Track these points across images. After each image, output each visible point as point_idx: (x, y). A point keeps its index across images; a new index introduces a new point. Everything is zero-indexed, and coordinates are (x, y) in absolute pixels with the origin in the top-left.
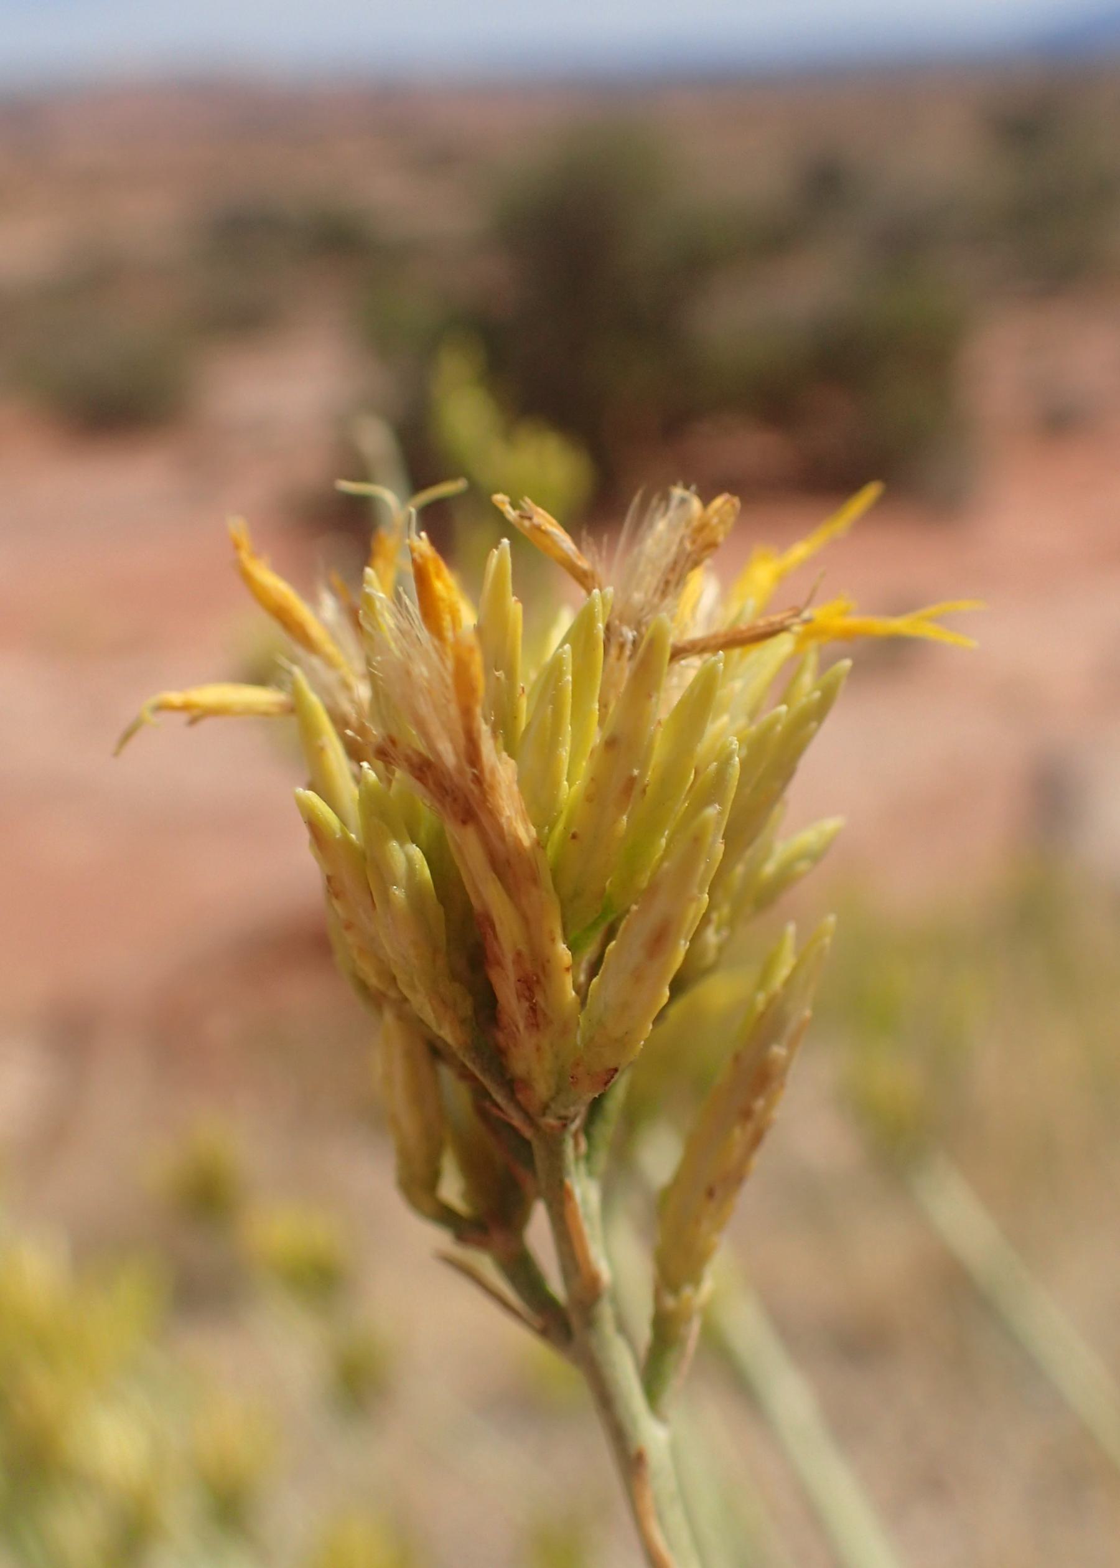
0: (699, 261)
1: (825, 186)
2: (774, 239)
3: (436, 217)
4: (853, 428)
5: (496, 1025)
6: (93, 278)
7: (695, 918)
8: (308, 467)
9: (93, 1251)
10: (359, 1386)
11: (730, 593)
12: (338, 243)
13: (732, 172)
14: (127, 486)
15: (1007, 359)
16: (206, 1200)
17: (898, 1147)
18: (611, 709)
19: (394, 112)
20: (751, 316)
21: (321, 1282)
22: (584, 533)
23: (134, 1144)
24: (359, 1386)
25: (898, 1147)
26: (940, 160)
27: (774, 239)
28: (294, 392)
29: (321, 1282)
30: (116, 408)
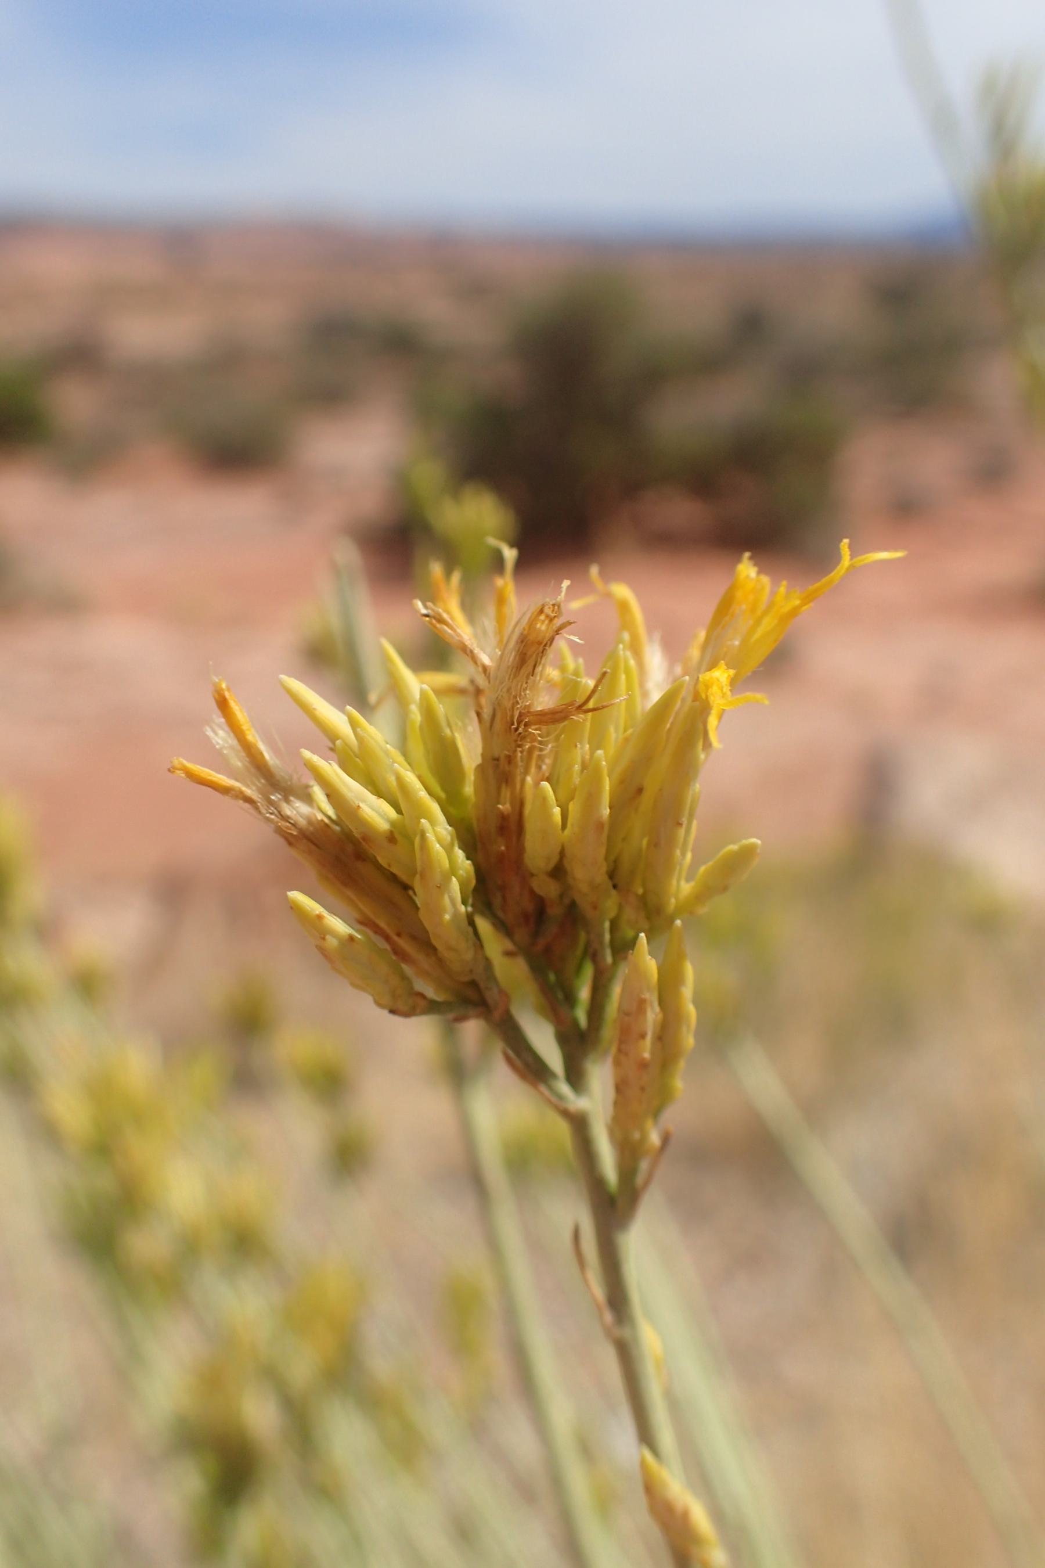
0: (654, 376)
2: (710, 363)
3: (473, 334)
4: (759, 501)
6: (226, 359)
7: (513, 632)
9: (175, 1044)
10: (349, 1157)
11: (635, 636)
12: (400, 345)
13: (682, 312)
14: (238, 509)
15: (872, 459)
16: (247, 1023)
18: (382, 924)
19: (444, 253)
20: (690, 418)
21: (330, 1084)
23: (206, 971)
24: (349, 1157)
26: (835, 314)
27: (710, 363)
28: (362, 450)
29: (330, 1084)
30: (236, 453)
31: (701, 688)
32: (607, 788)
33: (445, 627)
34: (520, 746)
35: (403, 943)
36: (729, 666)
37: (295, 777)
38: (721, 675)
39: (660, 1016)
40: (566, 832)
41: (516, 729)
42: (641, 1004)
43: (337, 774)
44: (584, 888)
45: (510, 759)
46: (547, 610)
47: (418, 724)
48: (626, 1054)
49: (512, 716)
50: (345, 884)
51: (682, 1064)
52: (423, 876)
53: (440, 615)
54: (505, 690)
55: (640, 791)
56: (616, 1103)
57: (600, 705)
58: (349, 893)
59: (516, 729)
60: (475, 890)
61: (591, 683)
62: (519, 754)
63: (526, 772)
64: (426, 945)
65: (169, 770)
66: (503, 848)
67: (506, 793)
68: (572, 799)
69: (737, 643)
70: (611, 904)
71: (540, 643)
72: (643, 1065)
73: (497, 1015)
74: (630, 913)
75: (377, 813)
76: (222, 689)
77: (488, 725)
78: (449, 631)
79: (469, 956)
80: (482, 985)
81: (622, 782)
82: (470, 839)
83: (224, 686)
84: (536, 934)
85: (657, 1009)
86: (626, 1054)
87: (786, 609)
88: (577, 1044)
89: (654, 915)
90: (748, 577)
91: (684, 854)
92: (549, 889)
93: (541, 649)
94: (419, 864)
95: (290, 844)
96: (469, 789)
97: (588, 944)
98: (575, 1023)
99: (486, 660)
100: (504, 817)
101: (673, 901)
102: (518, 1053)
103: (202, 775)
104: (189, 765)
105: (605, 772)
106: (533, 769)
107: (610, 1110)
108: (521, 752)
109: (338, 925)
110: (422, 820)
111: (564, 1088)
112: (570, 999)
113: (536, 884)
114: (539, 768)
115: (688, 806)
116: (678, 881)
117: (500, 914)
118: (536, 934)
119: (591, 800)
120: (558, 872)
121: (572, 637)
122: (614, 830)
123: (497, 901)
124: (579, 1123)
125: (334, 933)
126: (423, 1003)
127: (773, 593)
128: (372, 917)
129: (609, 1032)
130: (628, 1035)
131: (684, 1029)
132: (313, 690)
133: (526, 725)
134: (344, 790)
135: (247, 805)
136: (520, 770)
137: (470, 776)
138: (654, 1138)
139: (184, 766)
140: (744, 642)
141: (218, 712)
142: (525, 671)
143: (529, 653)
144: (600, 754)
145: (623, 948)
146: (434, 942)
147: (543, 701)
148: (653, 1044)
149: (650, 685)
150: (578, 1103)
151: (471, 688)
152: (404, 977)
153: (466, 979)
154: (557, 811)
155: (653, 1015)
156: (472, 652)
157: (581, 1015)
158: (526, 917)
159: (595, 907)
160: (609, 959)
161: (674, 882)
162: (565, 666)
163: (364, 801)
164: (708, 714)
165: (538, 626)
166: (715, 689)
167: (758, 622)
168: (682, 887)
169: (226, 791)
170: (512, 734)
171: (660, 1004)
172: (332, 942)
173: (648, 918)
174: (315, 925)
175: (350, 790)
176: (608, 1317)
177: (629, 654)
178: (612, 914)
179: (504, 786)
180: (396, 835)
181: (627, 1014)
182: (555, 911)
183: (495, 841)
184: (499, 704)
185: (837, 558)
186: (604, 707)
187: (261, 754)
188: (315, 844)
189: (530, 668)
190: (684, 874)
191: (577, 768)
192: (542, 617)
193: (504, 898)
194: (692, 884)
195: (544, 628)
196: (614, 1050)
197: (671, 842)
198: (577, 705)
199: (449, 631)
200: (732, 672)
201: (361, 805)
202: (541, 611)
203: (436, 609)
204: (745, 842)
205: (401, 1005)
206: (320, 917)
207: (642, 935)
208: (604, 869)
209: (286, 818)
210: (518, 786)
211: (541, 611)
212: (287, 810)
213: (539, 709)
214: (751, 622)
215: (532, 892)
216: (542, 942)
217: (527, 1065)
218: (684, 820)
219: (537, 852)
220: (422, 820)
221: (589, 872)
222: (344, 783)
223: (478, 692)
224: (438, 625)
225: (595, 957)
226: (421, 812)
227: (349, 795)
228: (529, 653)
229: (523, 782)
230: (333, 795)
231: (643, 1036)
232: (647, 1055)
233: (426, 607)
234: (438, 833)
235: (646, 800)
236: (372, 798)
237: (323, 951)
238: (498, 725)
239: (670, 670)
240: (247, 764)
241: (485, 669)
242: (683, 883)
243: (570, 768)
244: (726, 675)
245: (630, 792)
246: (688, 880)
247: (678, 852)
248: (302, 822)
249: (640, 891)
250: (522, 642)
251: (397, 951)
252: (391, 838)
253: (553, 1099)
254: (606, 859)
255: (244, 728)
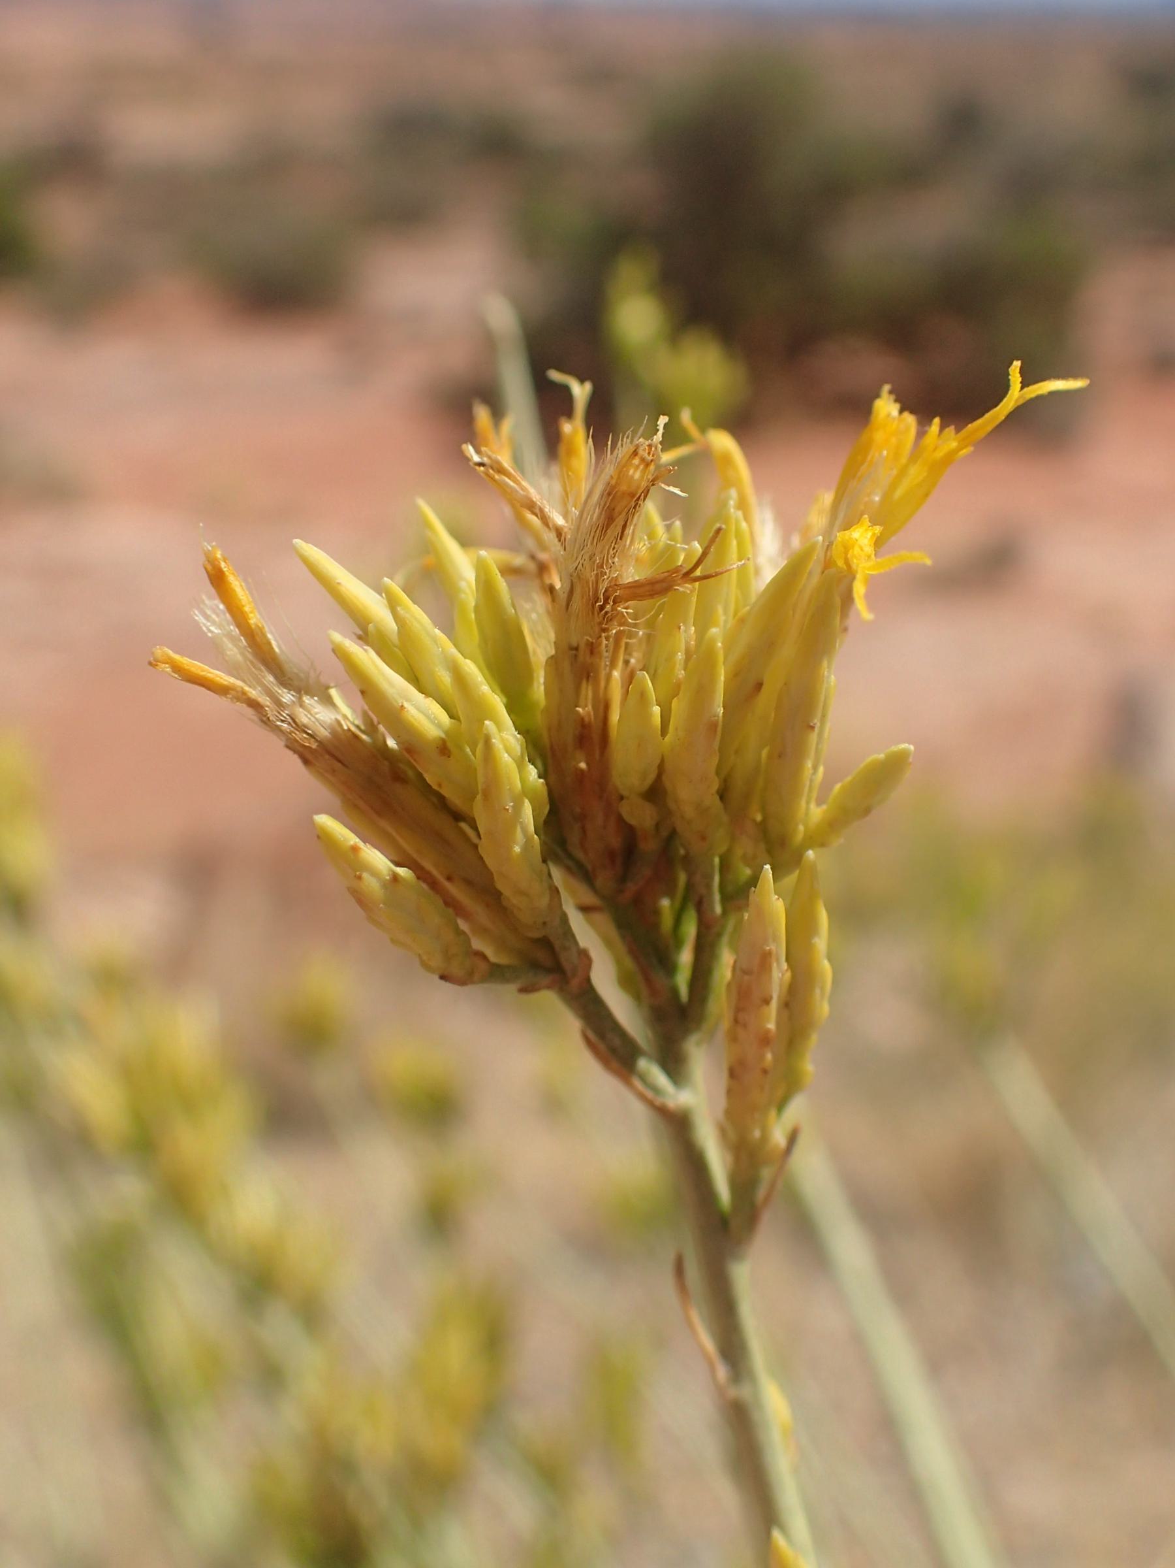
0: (835, 190)
1: (962, 124)
5: (612, 869)
6: (267, 163)
8: (457, 359)
12: (499, 146)
14: (285, 362)
15: (1123, 299)
17: (969, 1022)
18: (428, 865)
20: (884, 244)
21: (436, 1110)
22: (443, 736)
25: (969, 1022)
27: (906, 174)
28: (456, 287)
29: (436, 1110)
30: (280, 290)
31: (836, 550)
32: (722, 678)
33: (507, 480)
34: (604, 630)
35: (453, 889)
36: (874, 522)
37: (312, 674)
38: (862, 536)
39: (788, 975)
40: (667, 738)
41: (602, 608)
42: (765, 959)
43: (376, 666)
44: (689, 812)
45: (592, 648)
46: (641, 452)
47: (473, 603)
48: (745, 1026)
49: (596, 590)
50: (379, 813)
51: (814, 1039)
52: (486, 795)
53: (498, 463)
54: (586, 557)
55: (759, 686)
56: (730, 1092)
57: (707, 573)
58: (384, 824)
59: (602, 608)
60: (546, 822)
61: (697, 547)
62: (605, 642)
63: (613, 665)
64: (487, 891)
65: (150, 664)
66: (583, 765)
67: (587, 691)
68: (676, 694)
69: (877, 499)
70: (720, 841)
71: (632, 495)
72: (765, 1040)
73: (575, 983)
74: (745, 846)
75: (426, 716)
76: (216, 559)
77: (564, 604)
78: (512, 483)
79: (544, 902)
80: (557, 944)
81: (736, 674)
82: (540, 749)
83: (219, 555)
84: (623, 879)
85: (785, 966)
86: (745, 1026)
87: (939, 454)
88: (675, 1020)
89: (779, 848)
90: (889, 415)
91: (815, 768)
92: (641, 816)
93: (633, 504)
94: (481, 779)
95: (306, 762)
96: (539, 690)
97: (690, 886)
98: (675, 992)
99: (560, 521)
100: (583, 725)
101: (801, 828)
102: (602, 1036)
103: (193, 669)
104: (177, 657)
105: (721, 658)
106: (620, 663)
107: (722, 1102)
108: (607, 638)
109: (377, 859)
110: (487, 722)
111: (660, 1078)
112: (668, 966)
113: (625, 810)
114: (627, 662)
115: (821, 704)
116: (808, 803)
117: (579, 854)
118: (623, 879)
119: (702, 692)
120: (656, 793)
121: (672, 489)
122: (726, 734)
123: (574, 837)
124: (678, 1125)
125: (374, 873)
126: (483, 966)
127: (921, 434)
128: (415, 856)
129: (719, 1003)
130: (747, 996)
131: (818, 991)
132: (336, 560)
133: (615, 602)
134: (384, 686)
135: (250, 712)
136: (604, 662)
137: (540, 678)
138: (779, 1137)
139: (170, 658)
140: (886, 496)
141: (212, 590)
142: (615, 529)
143: (617, 510)
144: (717, 626)
145: (738, 895)
146: (499, 885)
147: (631, 574)
148: (779, 1013)
149: (762, 560)
150: (680, 1098)
151: (532, 566)
152: (459, 932)
153: (536, 935)
154: (657, 710)
155: (780, 974)
156: (541, 510)
157: (682, 980)
158: (611, 855)
159: (703, 838)
160: (718, 909)
161: (803, 804)
162: (654, 536)
163: (408, 700)
164: (854, 578)
165: (631, 472)
166: (856, 550)
167: (903, 472)
168: (811, 812)
169: (222, 690)
170: (594, 615)
171: (787, 960)
172: (371, 884)
173: (769, 852)
174: (349, 861)
175: (391, 684)
176: (722, 1372)
177: (740, 514)
178: (723, 849)
179: (584, 682)
180: (450, 745)
181: (746, 972)
182: (649, 846)
183: (572, 752)
184: (579, 577)
185: (1003, 389)
186: (717, 574)
187: (269, 644)
188: (340, 761)
189: (619, 529)
190: (815, 794)
191: (680, 656)
192: (636, 461)
193: (584, 830)
194: (824, 807)
195: (637, 475)
196: (726, 1024)
197: (799, 753)
198: (685, 571)
199: (512, 483)
200: (878, 529)
201: (406, 705)
202: (635, 453)
203: (494, 456)
204: (894, 748)
205: (456, 970)
206: (355, 849)
207: (768, 867)
208: (715, 786)
209: (302, 729)
210: (603, 684)
211: (635, 453)
212: (303, 718)
213: (630, 580)
214: (895, 472)
215: (620, 819)
216: (631, 888)
217: (613, 1051)
218: (816, 721)
219: (628, 767)
220: (487, 722)
221: (692, 793)
222: (383, 675)
223: (542, 568)
224: (497, 477)
225: (701, 906)
226: (480, 712)
227: (390, 692)
228: (615, 512)
229: (609, 677)
230: (367, 691)
231: (767, 1001)
232: (771, 1026)
233: (478, 452)
234: (506, 740)
235: (766, 700)
236: (419, 697)
237: (360, 898)
238: (577, 603)
239: (786, 541)
240: (250, 657)
241: (559, 533)
242: (813, 806)
243: (670, 657)
244: (869, 534)
245: (746, 689)
246: (819, 802)
247: (809, 764)
248: (324, 733)
249: (759, 818)
250: (609, 494)
251: (450, 902)
252: (443, 749)
253: (649, 1094)
254: (717, 773)
255: (247, 609)
